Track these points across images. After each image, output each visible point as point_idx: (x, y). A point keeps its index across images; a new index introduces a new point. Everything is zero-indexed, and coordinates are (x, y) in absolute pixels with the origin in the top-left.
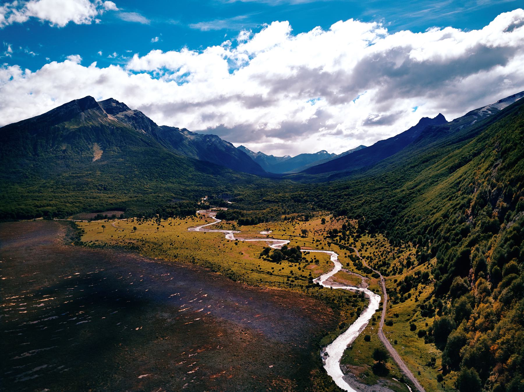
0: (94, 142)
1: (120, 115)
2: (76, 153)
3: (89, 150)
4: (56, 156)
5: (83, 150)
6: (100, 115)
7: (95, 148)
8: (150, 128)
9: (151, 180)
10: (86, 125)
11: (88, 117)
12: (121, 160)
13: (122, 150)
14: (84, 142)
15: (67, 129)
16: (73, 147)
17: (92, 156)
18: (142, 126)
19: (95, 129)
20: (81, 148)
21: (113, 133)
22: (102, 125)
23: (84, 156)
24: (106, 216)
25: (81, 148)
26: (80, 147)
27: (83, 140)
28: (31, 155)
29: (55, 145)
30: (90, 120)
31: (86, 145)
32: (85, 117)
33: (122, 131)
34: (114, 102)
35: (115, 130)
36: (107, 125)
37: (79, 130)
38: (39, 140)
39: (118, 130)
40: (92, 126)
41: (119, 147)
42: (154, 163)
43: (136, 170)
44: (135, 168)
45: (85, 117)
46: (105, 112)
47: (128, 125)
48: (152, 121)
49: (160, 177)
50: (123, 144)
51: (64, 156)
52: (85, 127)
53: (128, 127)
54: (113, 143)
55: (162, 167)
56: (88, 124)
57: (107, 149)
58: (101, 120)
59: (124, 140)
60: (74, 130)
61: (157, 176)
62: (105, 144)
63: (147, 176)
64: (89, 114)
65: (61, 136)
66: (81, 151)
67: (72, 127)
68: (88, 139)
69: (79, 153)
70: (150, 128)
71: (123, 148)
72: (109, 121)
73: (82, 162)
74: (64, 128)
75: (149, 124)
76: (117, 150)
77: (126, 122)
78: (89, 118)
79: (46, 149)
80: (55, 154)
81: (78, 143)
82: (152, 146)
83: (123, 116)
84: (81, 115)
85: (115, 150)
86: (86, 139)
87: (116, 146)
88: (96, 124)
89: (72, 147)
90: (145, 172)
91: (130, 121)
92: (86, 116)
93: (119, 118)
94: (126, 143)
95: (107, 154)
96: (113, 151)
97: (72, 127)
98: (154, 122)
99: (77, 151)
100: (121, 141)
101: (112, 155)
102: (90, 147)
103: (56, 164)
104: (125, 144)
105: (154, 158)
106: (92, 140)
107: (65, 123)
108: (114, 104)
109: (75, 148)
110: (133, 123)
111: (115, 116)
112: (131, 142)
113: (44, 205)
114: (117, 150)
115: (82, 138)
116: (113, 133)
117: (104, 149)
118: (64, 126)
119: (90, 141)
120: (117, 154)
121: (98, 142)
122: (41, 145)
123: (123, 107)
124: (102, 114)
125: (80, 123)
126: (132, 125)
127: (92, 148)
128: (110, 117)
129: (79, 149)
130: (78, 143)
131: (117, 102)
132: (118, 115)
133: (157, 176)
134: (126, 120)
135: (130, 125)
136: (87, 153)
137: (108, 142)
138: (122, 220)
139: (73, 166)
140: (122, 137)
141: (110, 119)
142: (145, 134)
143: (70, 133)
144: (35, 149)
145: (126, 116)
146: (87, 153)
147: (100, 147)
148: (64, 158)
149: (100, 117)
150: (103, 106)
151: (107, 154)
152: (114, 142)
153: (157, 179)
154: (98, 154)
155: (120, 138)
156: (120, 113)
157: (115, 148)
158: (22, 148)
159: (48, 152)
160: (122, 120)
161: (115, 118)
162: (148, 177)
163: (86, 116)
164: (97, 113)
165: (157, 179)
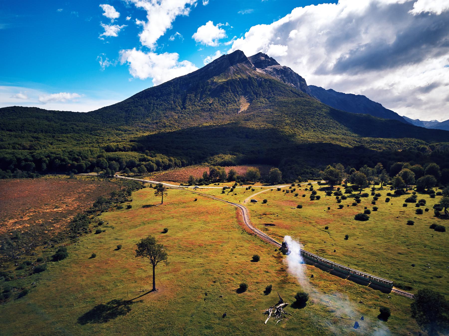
0: (241, 95)
1: (269, 69)
2: (222, 106)
3: (236, 102)
4: (202, 109)
5: (230, 102)
6: (248, 68)
7: (241, 101)
8: (299, 84)
9: (307, 129)
10: (234, 78)
11: (237, 70)
12: (269, 110)
13: (270, 101)
14: (231, 95)
15: (216, 82)
16: (220, 100)
17: (238, 107)
18: (291, 79)
19: (242, 81)
20: (228, 101)
21: (260, 85)
22: (250, 78)
23: (230, 108)
24: (232, 173)
25: (228, 101)
26: (227, 100)
27: (230, 93)
28: (179, 108)
29: (203, 98)
30: (238, 73)
31: (233, 97)
32: (234, 71)
33: (270, 82)
34: (263, 56)
35: (263, 83)
36: (256, 77)
37: (227, 83)
38: (188, 95)
39: (266, 82)
40: (240, 78)
41: (267, 98)
42: (308, 112)
43: (286, 119)
44: (286, 117)
45: (234, 71)
46: (253, 66)
47: (277, 78)
48: (301, 77)
49: (318, 127)
50: (271, 95)
51: (210, 109)
52: (233, 80)
53: (276, 79)
54: (260, 95)
55: (318, 117)
56: (236, 77)
57: (254, 101)
58: (250, 73)
59: (273, 91)
60: (222, 83)
61: (314, 125)
62: (252, 96)
63: (301, 125)
64: (238, 68)
65: (209, 91)
66: (227, 104)
67: (220, 80)
68: (235, 92)
69: (225, 105)
70: (299, 84)
71: (271, 99)
72: (258, 74)
73: (227, 114)
74: (213, 83)
75: (298, 80)
76: (264, 102)
77: (274, 75)
78: (238, 71)
79: (194, 102)
80: (201, 107)
81: (225, 96)
82: (303, 97)
83: (272, 70)
84: (230, 69)
85: (262, 102)
86: (233, 92)
87: (264, 98)
88: (244, 77)
89: (219, 100)
90: (298, 121)
91: (279, 75)
92: (235, 70)
93: (267, 71)
94: (274, 94)
95: (254, 105)
96: (261, 102)
97: (220, 80)
98: (303, 77)
99: (223, 104)
100: (269, 93)
101: (259, 107)
102: (236, 100)
103: (201, 116)
104: (273, 95)
105: (307, 108)
106: (239, 93)
107: (214, 77)
108: (263, 58)
109: (222, 100)
110: (282, 77)
111: (264, 70)
112: (279, 93)
113: (124, 147)
114: (264, 102)
115: (229, 91)
116: (260, 85)
117: (250, 101)
118: (213, 80)
119: (238, 94)
120: (264, 105)
121: (245, 95)
122: (190, 99)
123: (272, 61)
124: (250, 67)
125: (228, 76)
126: (280, 78)
127: (238, 101)
128: (258, 70)
129: (225, 102)
130: (225, 96)
131: (266, 56)
132: (266, 69)
133: (314, 125)
134: (275, 73)
135: (279, 78)
136: (234, 105)
137: (256, 94)
138: (275, 187)
139: (217, 117)
140: (270, 89)
141: (258, 72)
142: (294, 87)
143: (218, 86)
144: (184, 102)
145: (274, 69)
146: (234, 105)
147: (247, 100)
148: (210, 111)
149: (248, 70)
150: (251, 60)
151: (254, 105)
152: (262, 94)
153: (315, 129)
154: (244, 106)
155: (268, 90)
156: (268, 67)
157: (262, 99)
158: (172, 102)
159: (195, 105)
160: (270, 73)
161: (264, 71)
162: (303, 126)
163: (235, 70)
164: (246, 66)
165: (315, 129)
